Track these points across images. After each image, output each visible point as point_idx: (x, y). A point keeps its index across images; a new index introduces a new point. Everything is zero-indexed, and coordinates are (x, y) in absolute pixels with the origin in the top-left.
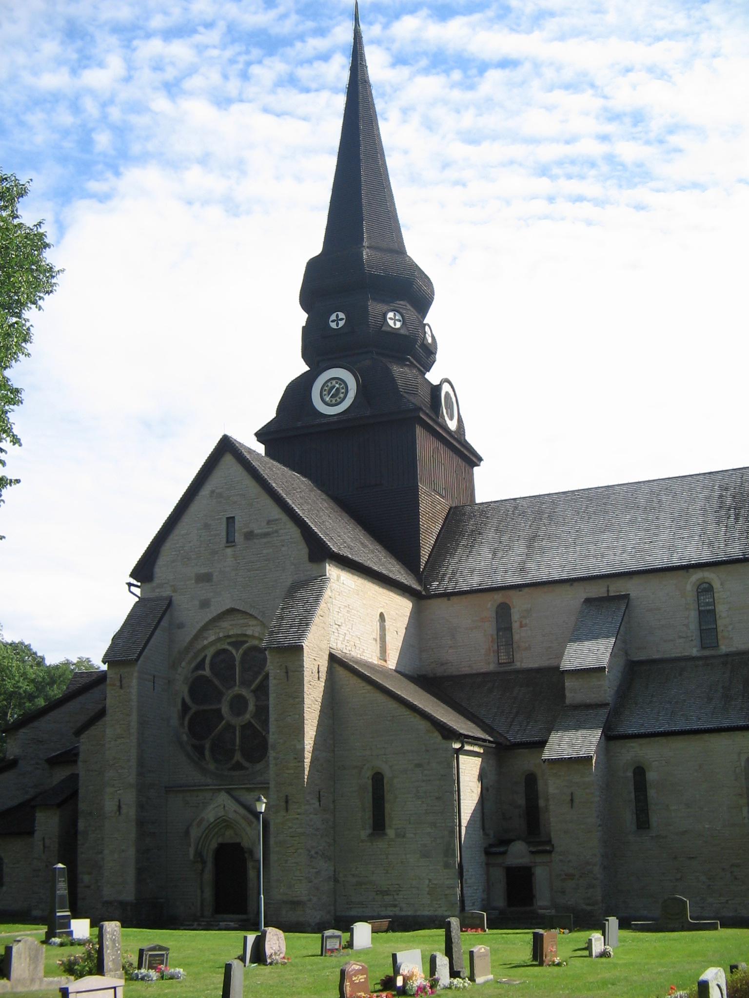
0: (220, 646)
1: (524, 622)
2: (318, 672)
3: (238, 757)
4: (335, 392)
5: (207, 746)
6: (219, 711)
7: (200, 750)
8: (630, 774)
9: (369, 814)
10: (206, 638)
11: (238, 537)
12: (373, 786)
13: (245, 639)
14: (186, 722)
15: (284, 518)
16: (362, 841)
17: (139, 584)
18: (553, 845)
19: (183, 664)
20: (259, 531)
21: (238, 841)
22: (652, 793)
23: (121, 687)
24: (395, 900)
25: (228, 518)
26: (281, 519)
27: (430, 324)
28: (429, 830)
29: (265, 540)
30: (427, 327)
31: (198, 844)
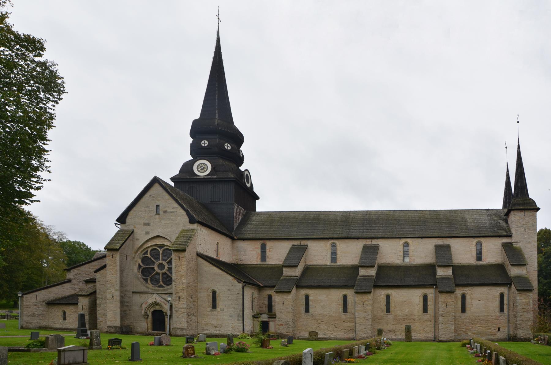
1: (270, 250)
2: (192, 258)
10: (148, 244)
11: (161, 212)
12: (212, 295)
14: (140, 271)
15: (179, 207)
16: (208, 311)
17: (120, 224)
18: (276, 316)
20: (170, 211)
21: (161, 309)
22: (310, 303)
23: (113, 258)
25: (157, 205)
26: (178, 208)
27: (242, 150)
28: (232, 309)
29: (172, 214)
30: (240, 151)
31: (146, 310)
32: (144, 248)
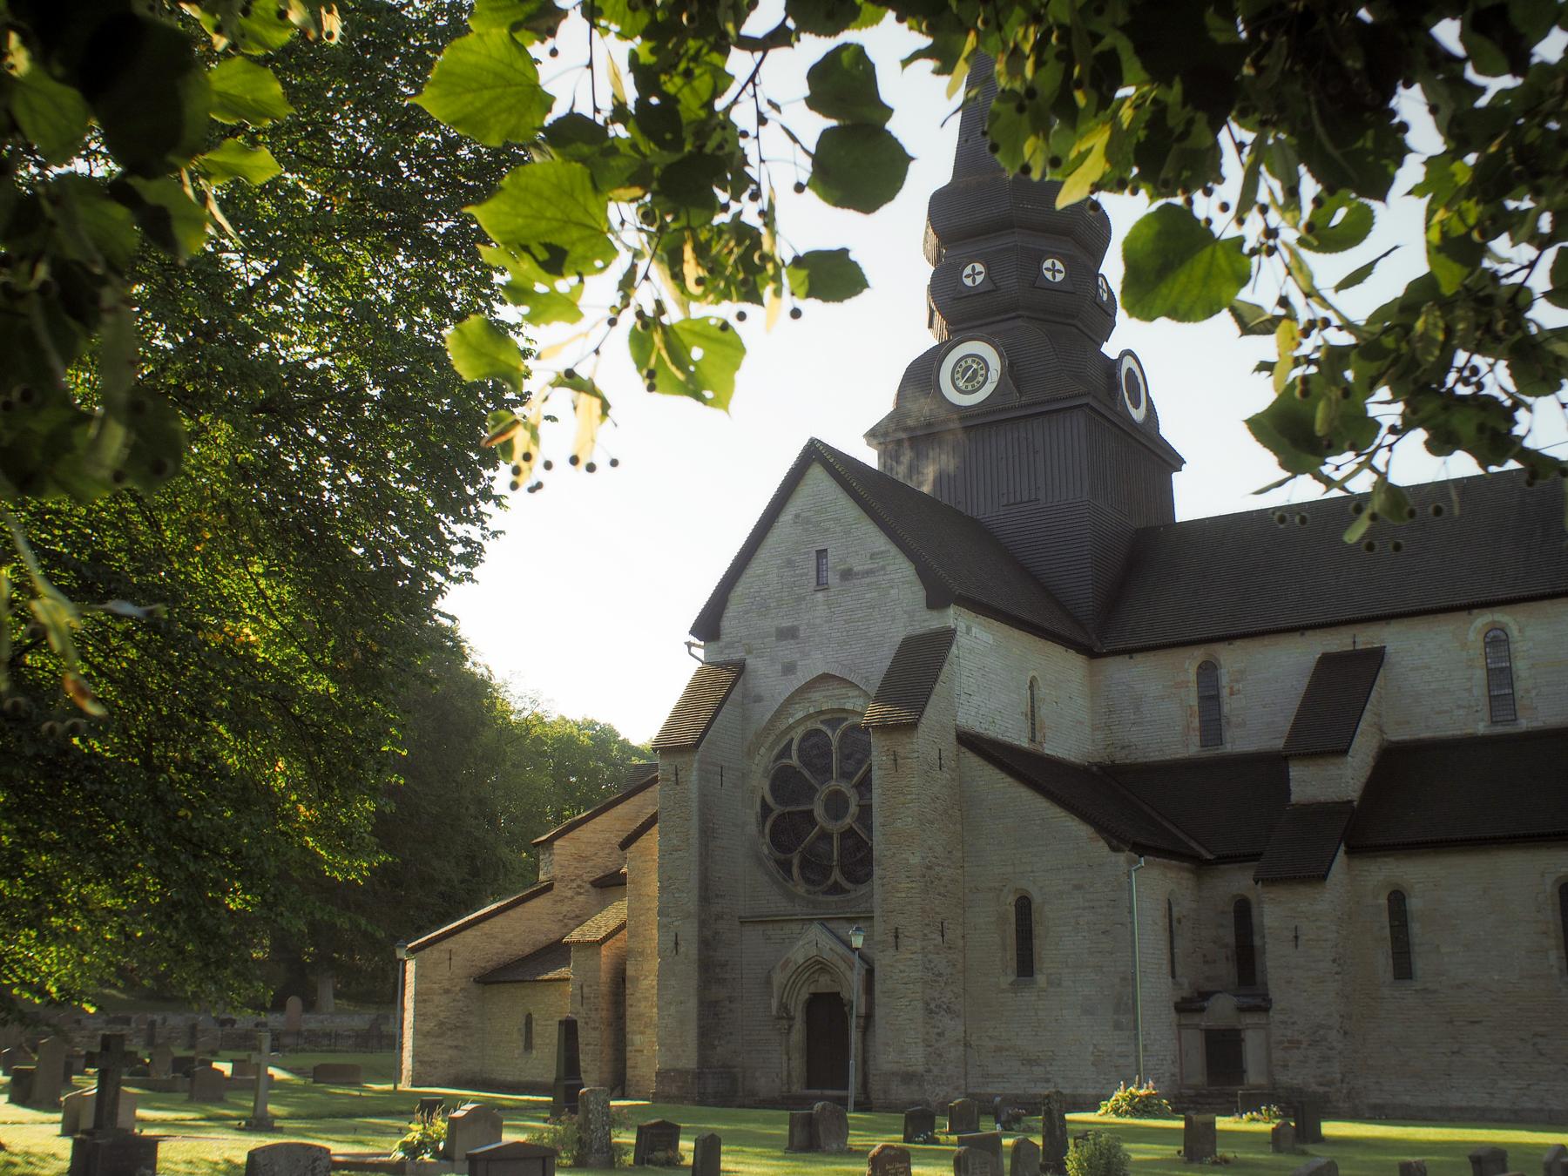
0: (811, 725)
3: (836, 875)
4: (971, 373)
5: (796, 861)
6: (809, 815)
7: (785, 866)
8: (1383, 901)
9: (1011, 954)
10: (792, 715)
11: (833, 579)
13: (844, 715)
14: (767, 831)
19: (762, 750)
20: (860, 568)
22: (1415, 928)
23: (677, 784)
24: (1048, 1073)
29: (867, 580)
32: (778, 732)
